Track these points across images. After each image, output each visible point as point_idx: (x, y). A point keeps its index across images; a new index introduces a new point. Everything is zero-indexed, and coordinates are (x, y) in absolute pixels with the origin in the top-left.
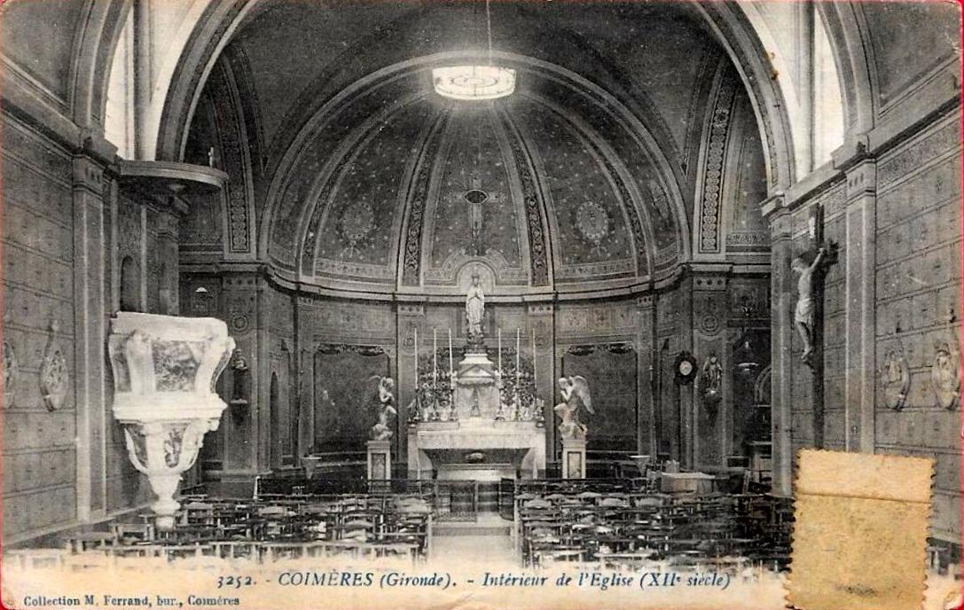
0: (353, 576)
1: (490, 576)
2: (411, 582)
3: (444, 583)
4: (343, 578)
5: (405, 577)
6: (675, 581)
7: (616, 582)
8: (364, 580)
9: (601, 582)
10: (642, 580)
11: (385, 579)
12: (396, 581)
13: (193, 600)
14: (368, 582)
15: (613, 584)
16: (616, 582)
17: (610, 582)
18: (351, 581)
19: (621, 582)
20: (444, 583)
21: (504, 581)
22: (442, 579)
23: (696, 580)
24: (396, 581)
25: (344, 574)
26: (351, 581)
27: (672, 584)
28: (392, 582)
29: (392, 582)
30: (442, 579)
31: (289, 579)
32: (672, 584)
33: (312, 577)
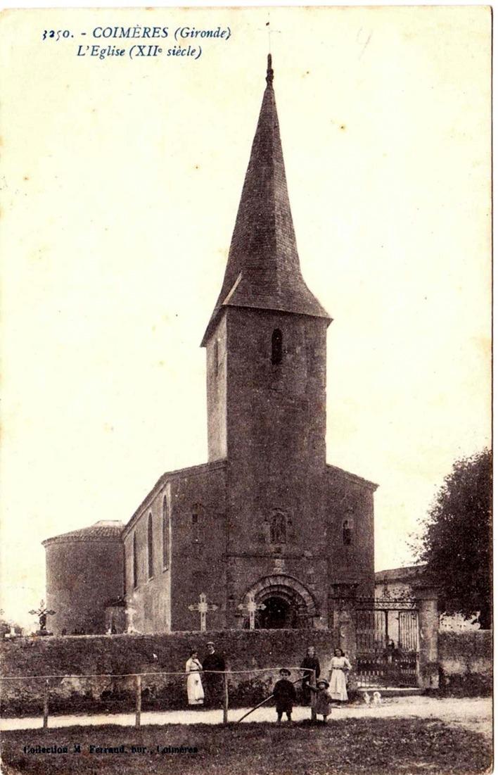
0: (152, 30)
1: (158, 48)
2: (199, 34)
3: (226, 35)
4: (145, 32)
5: (195, 31)
6: (157, 53)
7: (111, 52)
8: (161, 33)
9: (99, 52)
10: (199, 56)
11: (179, 32)
12: (188, 34)
13: (99, 33)
14: (164, 35)
15: (108, 55)
16: (111, 52)
17: (107, 52)
18: (151, 34)
19: (115, 52)
20: (226, 35)
21: (119, 52)
22: (195, 50)
23: (174, 51)
24: (188, 34)
25: (145, 29)
26: (151, 34)
27: (110, 47)
28: (184, 34)
29: (184, 34)
30: (195, 50)
31: (101, 33)
32: (155, 55)
33: (119, 31)
